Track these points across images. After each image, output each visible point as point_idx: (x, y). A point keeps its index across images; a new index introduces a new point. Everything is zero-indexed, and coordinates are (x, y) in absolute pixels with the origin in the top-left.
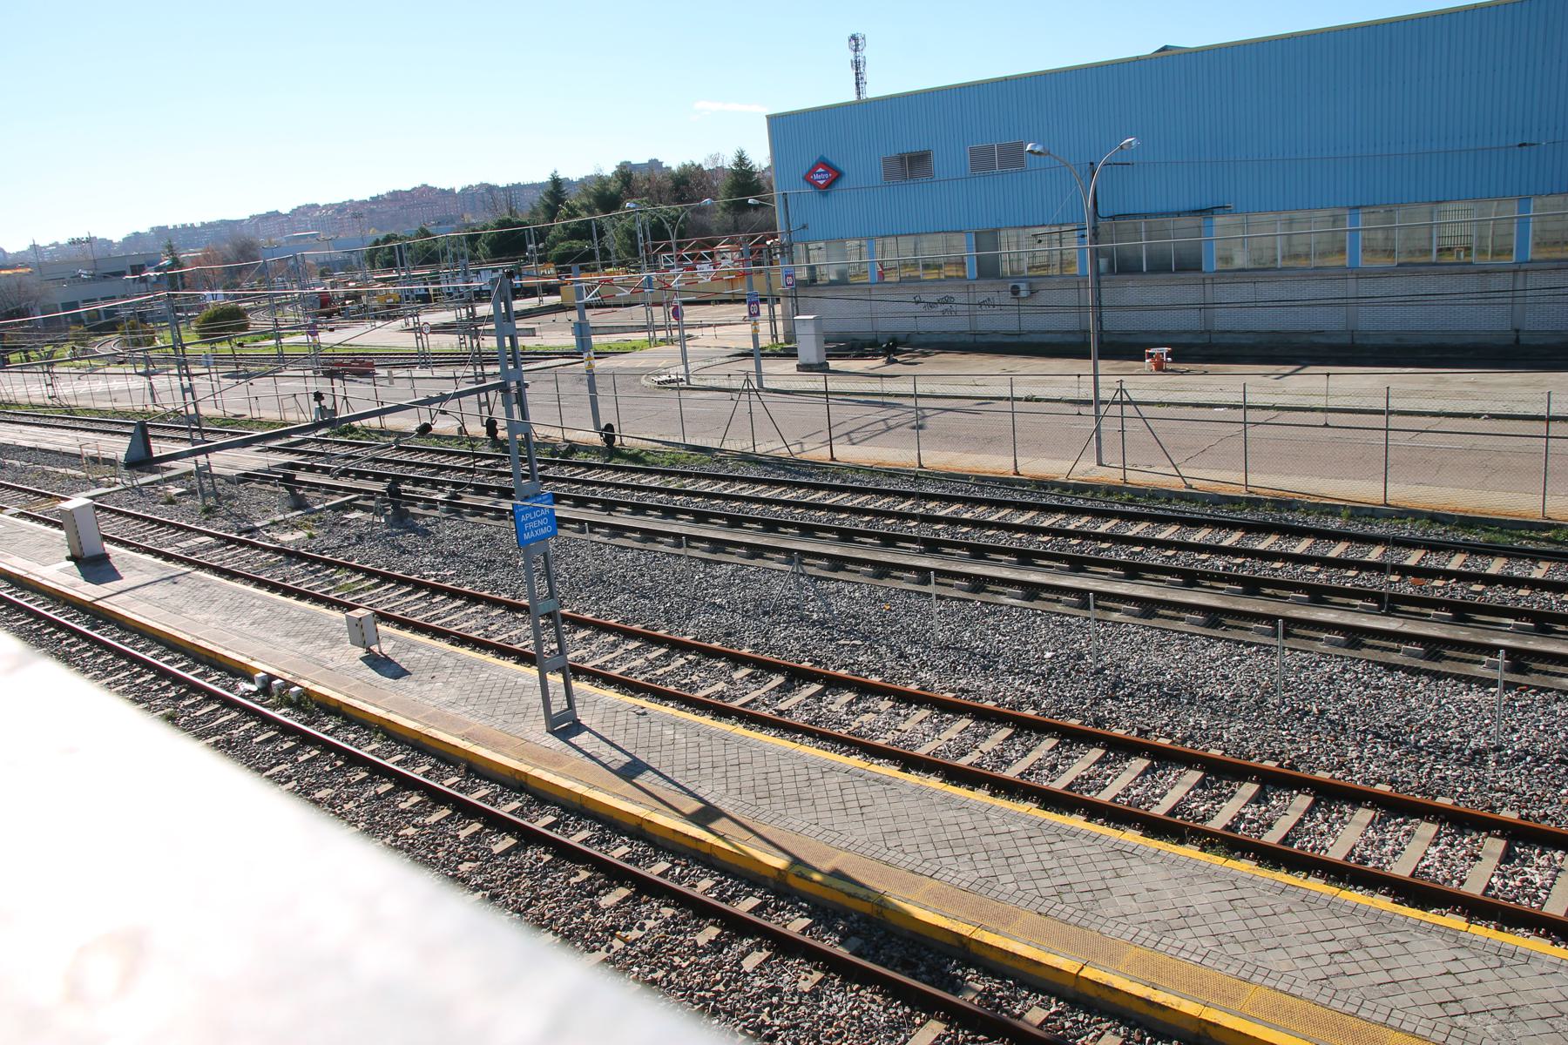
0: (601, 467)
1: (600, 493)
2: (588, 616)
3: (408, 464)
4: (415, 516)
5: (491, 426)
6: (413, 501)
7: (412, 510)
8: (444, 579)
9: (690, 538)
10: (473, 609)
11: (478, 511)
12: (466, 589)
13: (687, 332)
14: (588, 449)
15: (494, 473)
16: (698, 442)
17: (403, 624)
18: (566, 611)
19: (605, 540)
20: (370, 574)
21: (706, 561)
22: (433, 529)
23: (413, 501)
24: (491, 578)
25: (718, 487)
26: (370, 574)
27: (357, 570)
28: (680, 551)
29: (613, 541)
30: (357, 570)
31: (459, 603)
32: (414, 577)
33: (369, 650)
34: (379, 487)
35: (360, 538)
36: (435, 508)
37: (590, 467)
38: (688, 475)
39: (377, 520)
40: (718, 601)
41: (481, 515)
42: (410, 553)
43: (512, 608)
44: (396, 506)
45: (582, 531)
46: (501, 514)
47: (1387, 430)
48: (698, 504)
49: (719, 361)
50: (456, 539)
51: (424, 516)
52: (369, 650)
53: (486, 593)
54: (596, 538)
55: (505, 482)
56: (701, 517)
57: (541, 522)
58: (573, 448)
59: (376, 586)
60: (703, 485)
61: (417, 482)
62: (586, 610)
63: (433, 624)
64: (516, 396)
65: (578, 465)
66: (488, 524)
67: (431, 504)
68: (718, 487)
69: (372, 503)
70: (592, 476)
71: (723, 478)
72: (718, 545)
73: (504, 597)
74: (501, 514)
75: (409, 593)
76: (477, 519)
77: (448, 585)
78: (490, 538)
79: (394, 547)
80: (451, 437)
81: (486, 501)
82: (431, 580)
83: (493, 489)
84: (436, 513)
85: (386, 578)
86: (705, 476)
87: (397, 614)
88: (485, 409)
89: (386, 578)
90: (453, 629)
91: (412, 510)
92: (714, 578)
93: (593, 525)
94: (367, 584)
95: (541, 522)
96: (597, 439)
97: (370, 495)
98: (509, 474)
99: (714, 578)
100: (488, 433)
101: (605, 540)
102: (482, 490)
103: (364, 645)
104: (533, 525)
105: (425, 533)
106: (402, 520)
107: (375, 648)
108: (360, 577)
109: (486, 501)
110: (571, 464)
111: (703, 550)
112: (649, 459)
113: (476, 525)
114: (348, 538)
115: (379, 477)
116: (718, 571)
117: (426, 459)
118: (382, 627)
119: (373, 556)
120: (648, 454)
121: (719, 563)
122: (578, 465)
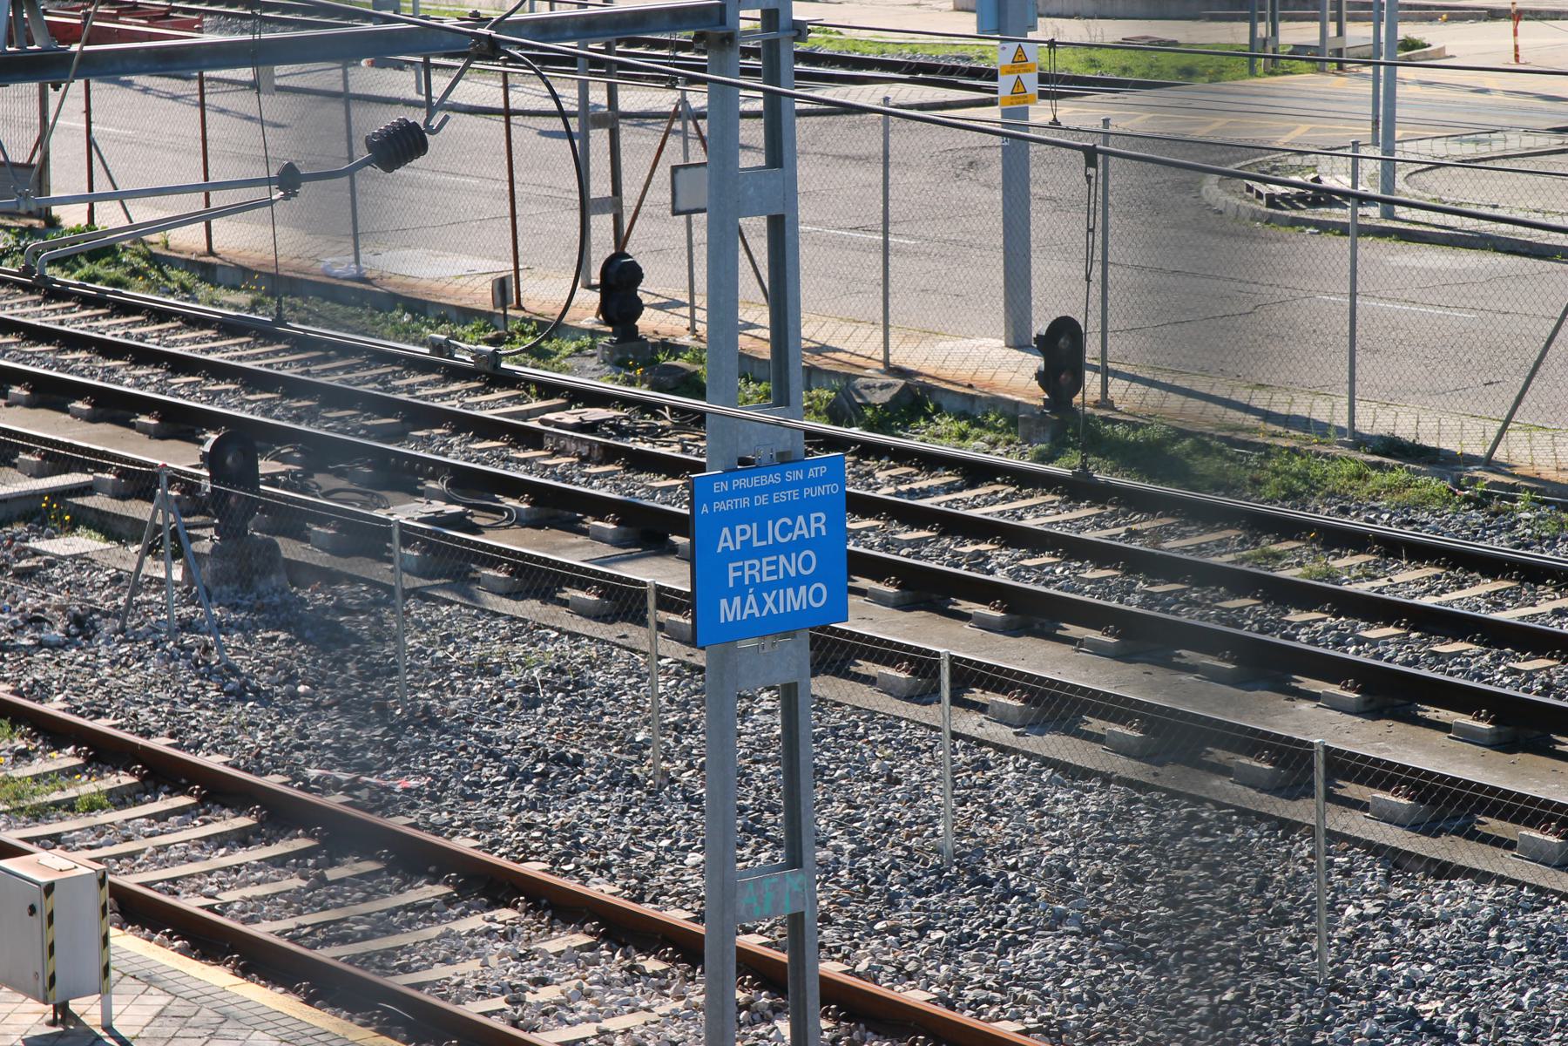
0: (1024, 480)
1: (1002, 567)
2: (916, 997)
3: (292, 388)
4: (295, 570)
5: (620, 286)
6: (292, 521)
7: (290, 549)
8: (383, 801)
9: (1344, 766)
10: (476, 922)
11: (539, 580)
12: (464, 844)
13: (1405, 30)
14: (974, 408)
15: (609, 454)
16: (1405, 428)
17: (205, 940)
18: (832, 968)
19: (1004, 735)
20: (104, 753)
21: (1397, 861)
22: (363, 625)
23: (292, 521)
24: (560, 816)
25: (1471, 596)
26: (104, 753)
27: (55, 733)
28: (1299, 811)
29: (1032, 743)
30: (55, 733)
31: (427, 892)
32: (273, 781)
33: (63, 1013)
34: (181, 457)
35: (82, 626)
36: (381, 555)
37: (976, 473)
38: (1356, 541)
39: (154, 569)
40: (1429, 1007)
41: (547, 596)
42: (263, 697)
43: (623, 930)
44: (231, 531)
45: (924, 694)
46: (624, 603)
47: (507, 113)
48: (1382, 645)
49: (1516, 143)
50: (442, 668)
51: (330, 578)
52: (63, 1013)
53: (534, 868)
54: (969, 723)
55: (653, 491)
56: (1391, 695)
57: (791, 566)
58: (916, 399)
59: (120, 799)
60: (1407, 582)
61: (319, 454)
62: (903, 974)
63: (324, 954)
64: (749, 202)
65: (930, 462)
66: (565, 631)
67: (371, 539)
68: (1471, 596)
69: (139, 510)
70: (983, 504)
71: (1491, 566)
72: (1448, 806)
73: (601, 889)
74: (624, 603)
75: (242, 839)
76: (530, 609)
77: (399, 823)
78: (567, 679)
79: (206, 672)
80: (466, 315)
81: (571, 551)
82: (335, 800)
83: (599, 507)
84: (381, 572)
85: (161, 774)
86: (1419, 553)
87: (191, 903)
88: (602, 225)
89: (161, 774)
90: (400, 982)
91: (290, 549)
92: (1425, 922)
93: (968, 675)
94: (87, 787)
95: (791, 566)
96: (1017, 375)
97: (139, 482)
98: (671, 467)
99: (1425, 922)
100: (606, 310)
101: (1004, 735)
102: (558, 508)
103: (49, 988)
104: (758, 570)
105: (325, 635)
106: (245, 579)
107: (87, 1009)
108: (66, 758)
109: (571, 551)
110: (901, 456)
111: (1387, 816)
112: (1204, 466)
113: (521, 629)
114: (35, 621)
115: (179, 423)
116: (1437, 898)
117: (365, 381)
118: (128, 944)
119: (130, 694)
120: (1203, 445)
121: (1444, 870)
122: (930, 462)
